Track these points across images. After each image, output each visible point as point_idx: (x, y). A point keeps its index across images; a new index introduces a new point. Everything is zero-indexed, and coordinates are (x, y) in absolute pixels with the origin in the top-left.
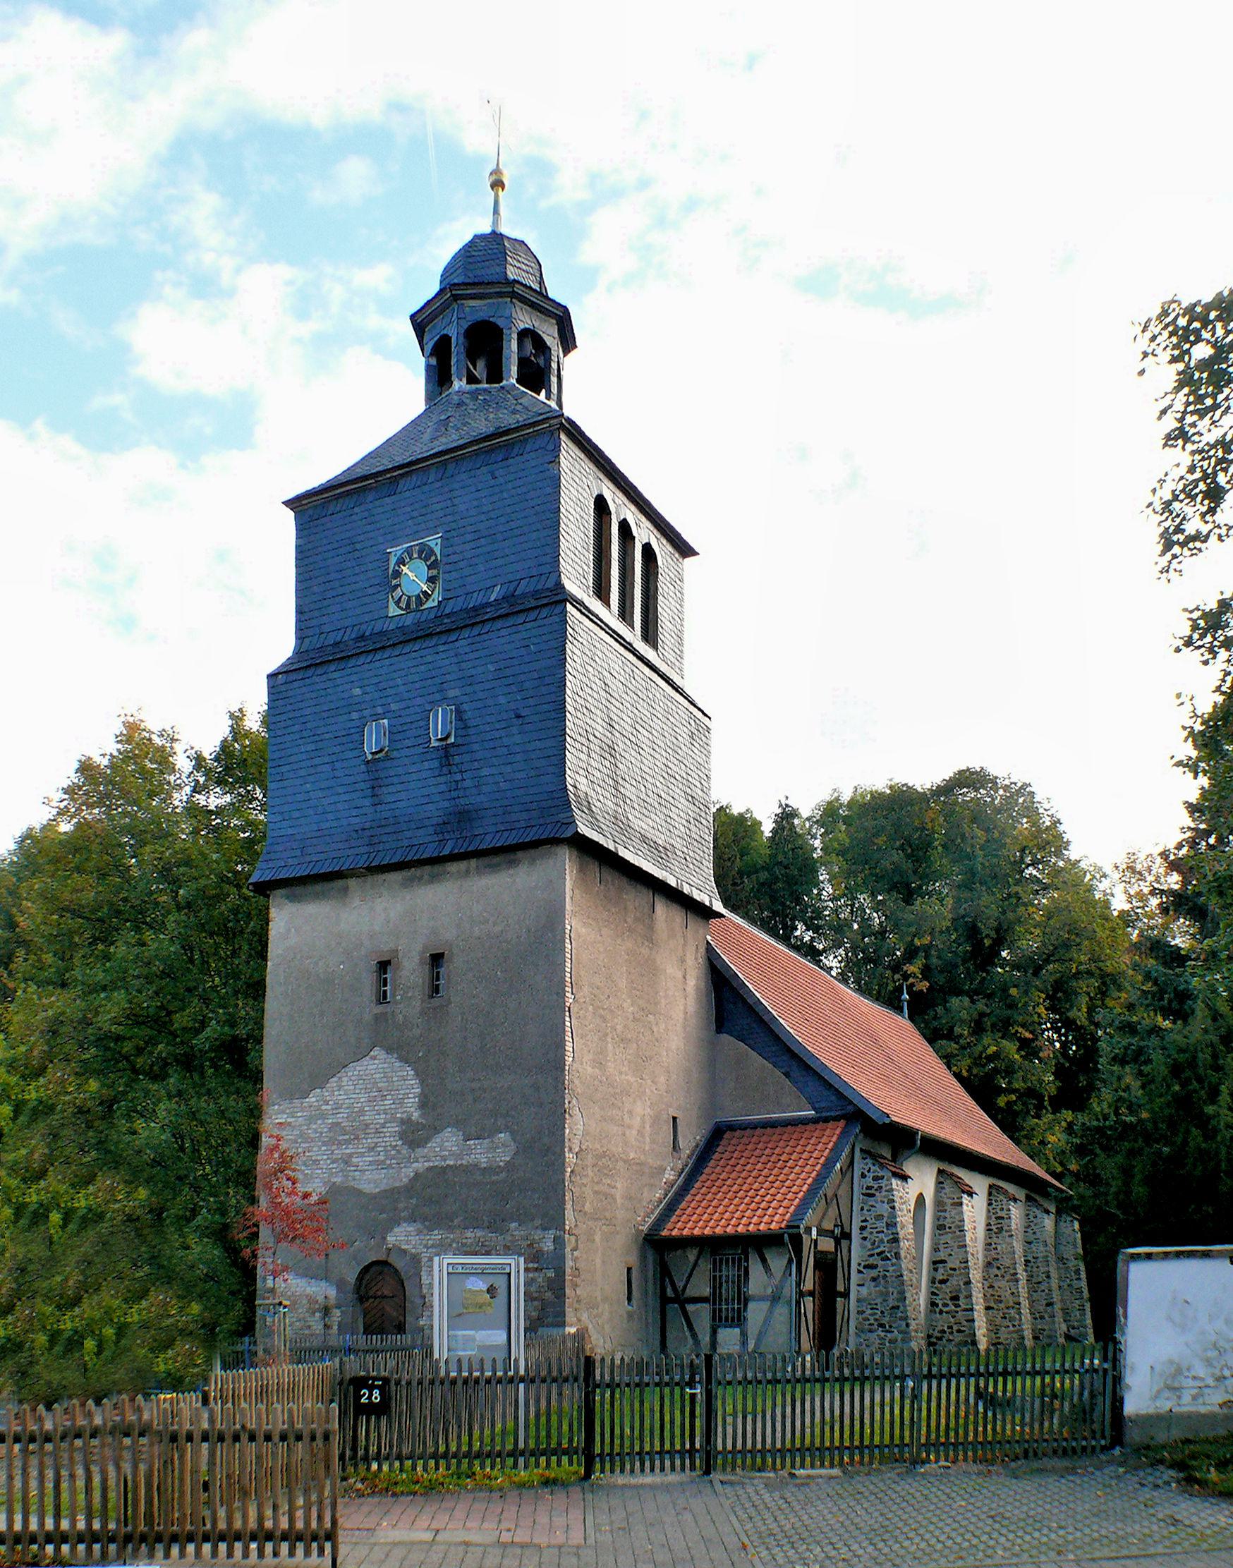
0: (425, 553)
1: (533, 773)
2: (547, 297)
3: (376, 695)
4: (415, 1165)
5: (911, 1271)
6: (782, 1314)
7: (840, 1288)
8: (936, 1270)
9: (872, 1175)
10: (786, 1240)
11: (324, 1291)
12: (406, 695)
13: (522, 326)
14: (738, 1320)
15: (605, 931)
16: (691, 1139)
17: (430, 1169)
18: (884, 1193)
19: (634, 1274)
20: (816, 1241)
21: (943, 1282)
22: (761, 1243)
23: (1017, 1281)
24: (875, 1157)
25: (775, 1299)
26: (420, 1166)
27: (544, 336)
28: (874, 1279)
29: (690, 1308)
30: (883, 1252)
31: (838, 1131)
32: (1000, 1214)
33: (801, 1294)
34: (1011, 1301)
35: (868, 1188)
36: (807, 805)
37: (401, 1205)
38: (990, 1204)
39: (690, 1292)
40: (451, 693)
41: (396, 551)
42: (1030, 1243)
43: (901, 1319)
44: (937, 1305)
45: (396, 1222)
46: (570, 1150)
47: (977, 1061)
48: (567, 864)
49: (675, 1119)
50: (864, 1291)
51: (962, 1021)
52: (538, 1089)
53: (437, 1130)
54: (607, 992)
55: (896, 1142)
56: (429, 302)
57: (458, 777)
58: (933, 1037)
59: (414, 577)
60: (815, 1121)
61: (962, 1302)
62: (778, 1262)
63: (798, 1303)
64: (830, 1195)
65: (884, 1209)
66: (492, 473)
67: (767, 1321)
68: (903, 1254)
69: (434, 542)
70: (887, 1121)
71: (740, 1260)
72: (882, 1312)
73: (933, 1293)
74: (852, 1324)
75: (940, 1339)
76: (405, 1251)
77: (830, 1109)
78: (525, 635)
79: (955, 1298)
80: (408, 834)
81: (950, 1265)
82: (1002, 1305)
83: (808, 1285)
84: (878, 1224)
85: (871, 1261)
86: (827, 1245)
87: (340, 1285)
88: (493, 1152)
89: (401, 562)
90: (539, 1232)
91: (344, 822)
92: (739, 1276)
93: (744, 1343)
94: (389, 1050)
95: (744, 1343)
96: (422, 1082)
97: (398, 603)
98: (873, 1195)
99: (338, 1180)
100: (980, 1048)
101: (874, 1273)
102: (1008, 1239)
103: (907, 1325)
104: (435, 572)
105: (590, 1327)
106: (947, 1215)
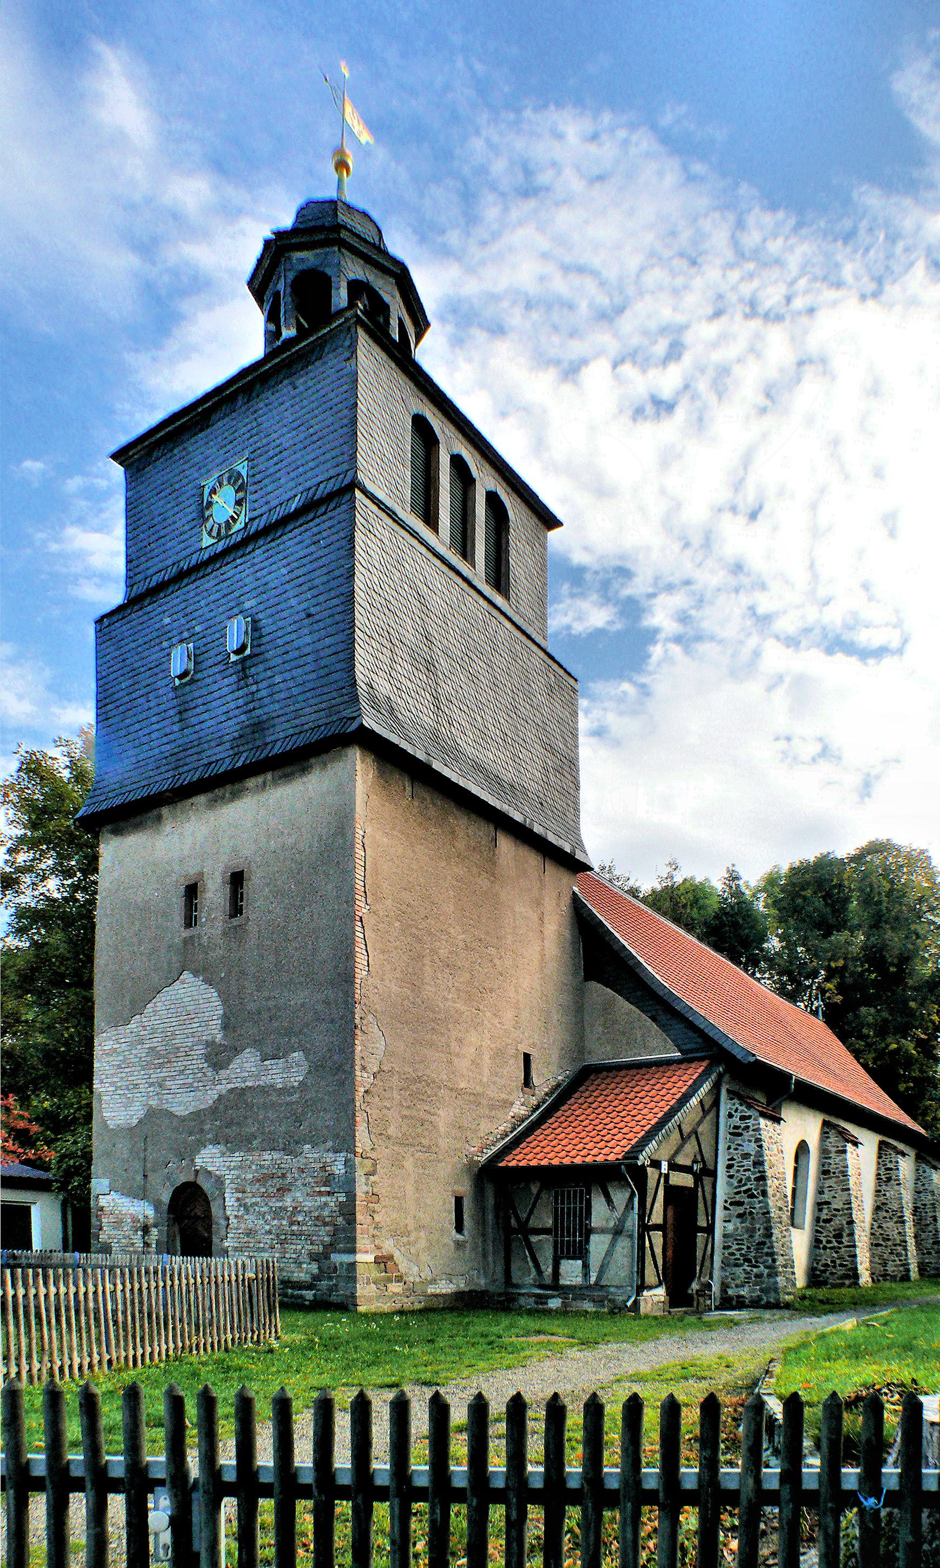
0: (234, 478)
1: (322, 672)
2: (385, 253)
3: (183, 621)
4: (218, 1087)
5: (780, 1209)
6: (624, 1247)
7: (702, 1222)
8: (820, 1210)
9: (739, 1115)
10: (627, 1173)
11: (145, 1210)
12: (208, 616)
13: (352, 276)
14: (581, 1252)
15: (418, 848)
16: (547, 1077)
17: (231, 1091)
18: (751, 1133)
19: (467, 1204)
20: (667, 1176)
21: (827, 1221)
22: (601, 1176)
23: (903, 1222)
24: (743, 1100)
25: (618, 1232)
26: (223, 1088)
27: (381, 292)
28: (740, 1216)
29: (534, 1239)
30: (750, 1190)
31: (700, 1071)
32: (889, 1166)
33: (645, 1228)
34: (898, 1239)
35: (735, 1127)
36: (752, 878)
37: (207, 1127)
38: (880, 1157)
39: (533, 1223)
40: (247, 605)
41: (210, 483)
42: (919, 1192)
43: (767, 1254)
44: (821, 1242)
45: (201, 1144)
46: (364, 1068)
47: (881, 1054)
48: (359, 769)
49: (527, 1057)
50: (730, 1227)
51: (869, 1026)
52: (329, 1004)
53: (237, 1051)
54: (423, 913)
55: (771, 1089)
56: (260, 261)
57: (254, 688)
58: (843, 1037)
59: (224, 504)
60: (679, 1062)
61: (845, 1240)
62: (620, 1197)
63: (641, 1238)
64: (687, 1129)
65: (751, 1148)
66: (292, 383)
67: (609, 1253)
68: (770, 1191)
69: (242, 468)
70: (752, 1059)
71: (581, 1191)
72: (748, 1248)
73: (817, 1231)
74: (717, 1259)
75: (824, 1271)
76: (210, 1172)
77: (697, 1050)
78: (315, 530)
79: (838, 1236)
80: (208, 753)
81: (834, 1206)
82: (890, 1243)
83: (657, 1217)
84: (745, 1162)
85: (738, 1198)
86: (682, 1180)
87: (157, 1205)
88: (288, 1072)
89: (213, 491)
90: (331, 1155)
91: (157, 751)
92: (581, 1209)
93: (586, 1275)
94: (196, 973)
95: (586, 1275)
96: (225, 1002)
97: (209, 534)
98: (740, 1135)
99: (154, 1103)
100: (883, 1045)
101: (741, 1210)
102: (896, 1187)
103: (774, 1261)
104: (241, 495)
105: (397, 1255)
106: (831, 1161)
